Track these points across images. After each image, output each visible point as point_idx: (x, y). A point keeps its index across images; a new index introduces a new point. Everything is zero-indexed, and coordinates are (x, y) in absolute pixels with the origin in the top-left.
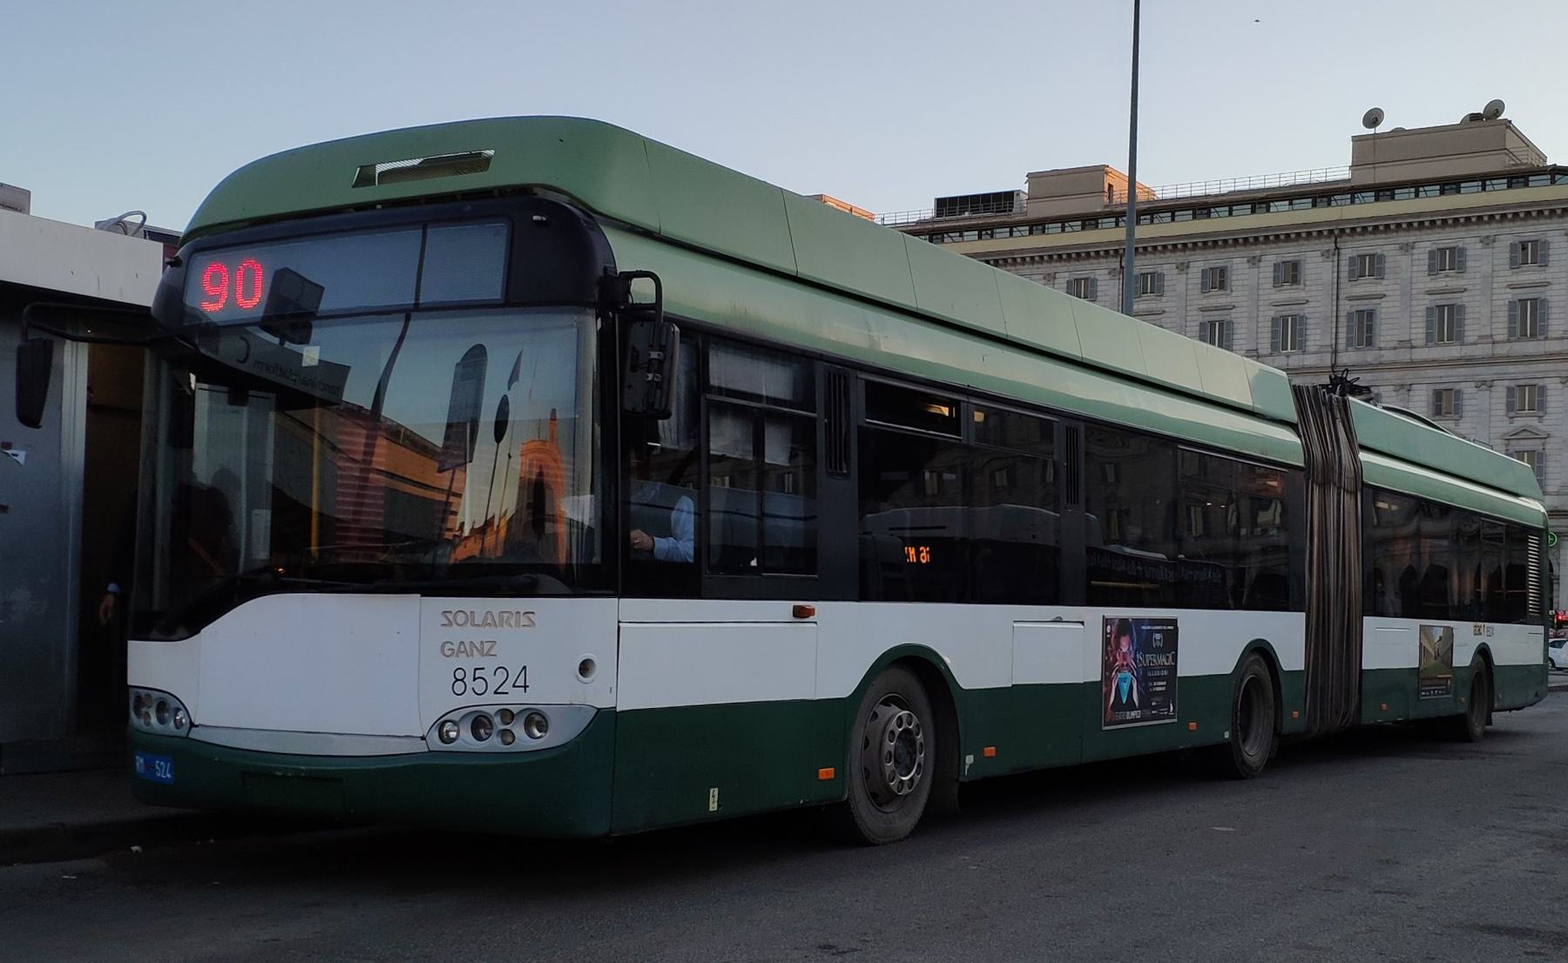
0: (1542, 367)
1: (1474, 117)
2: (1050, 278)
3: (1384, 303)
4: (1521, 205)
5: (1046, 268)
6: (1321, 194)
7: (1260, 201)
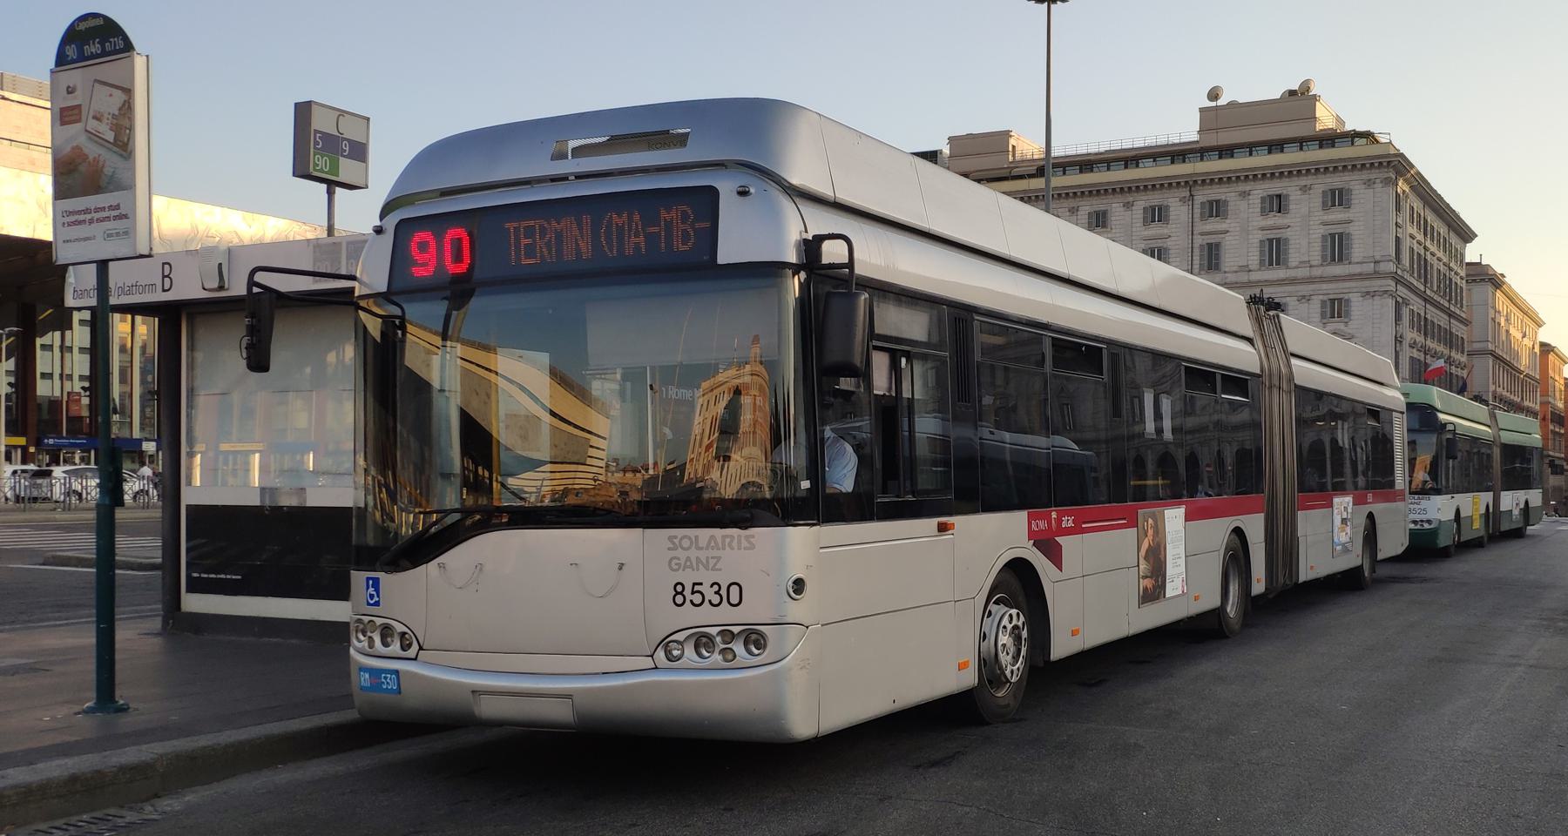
0: (1347, 284)
1: (1292, 93)
2: (1073, 211)
3: (1228, 237)
4: (1331, 161)
5: (1072, 203)
6: (1177, 153)
7: (1131, 159)
